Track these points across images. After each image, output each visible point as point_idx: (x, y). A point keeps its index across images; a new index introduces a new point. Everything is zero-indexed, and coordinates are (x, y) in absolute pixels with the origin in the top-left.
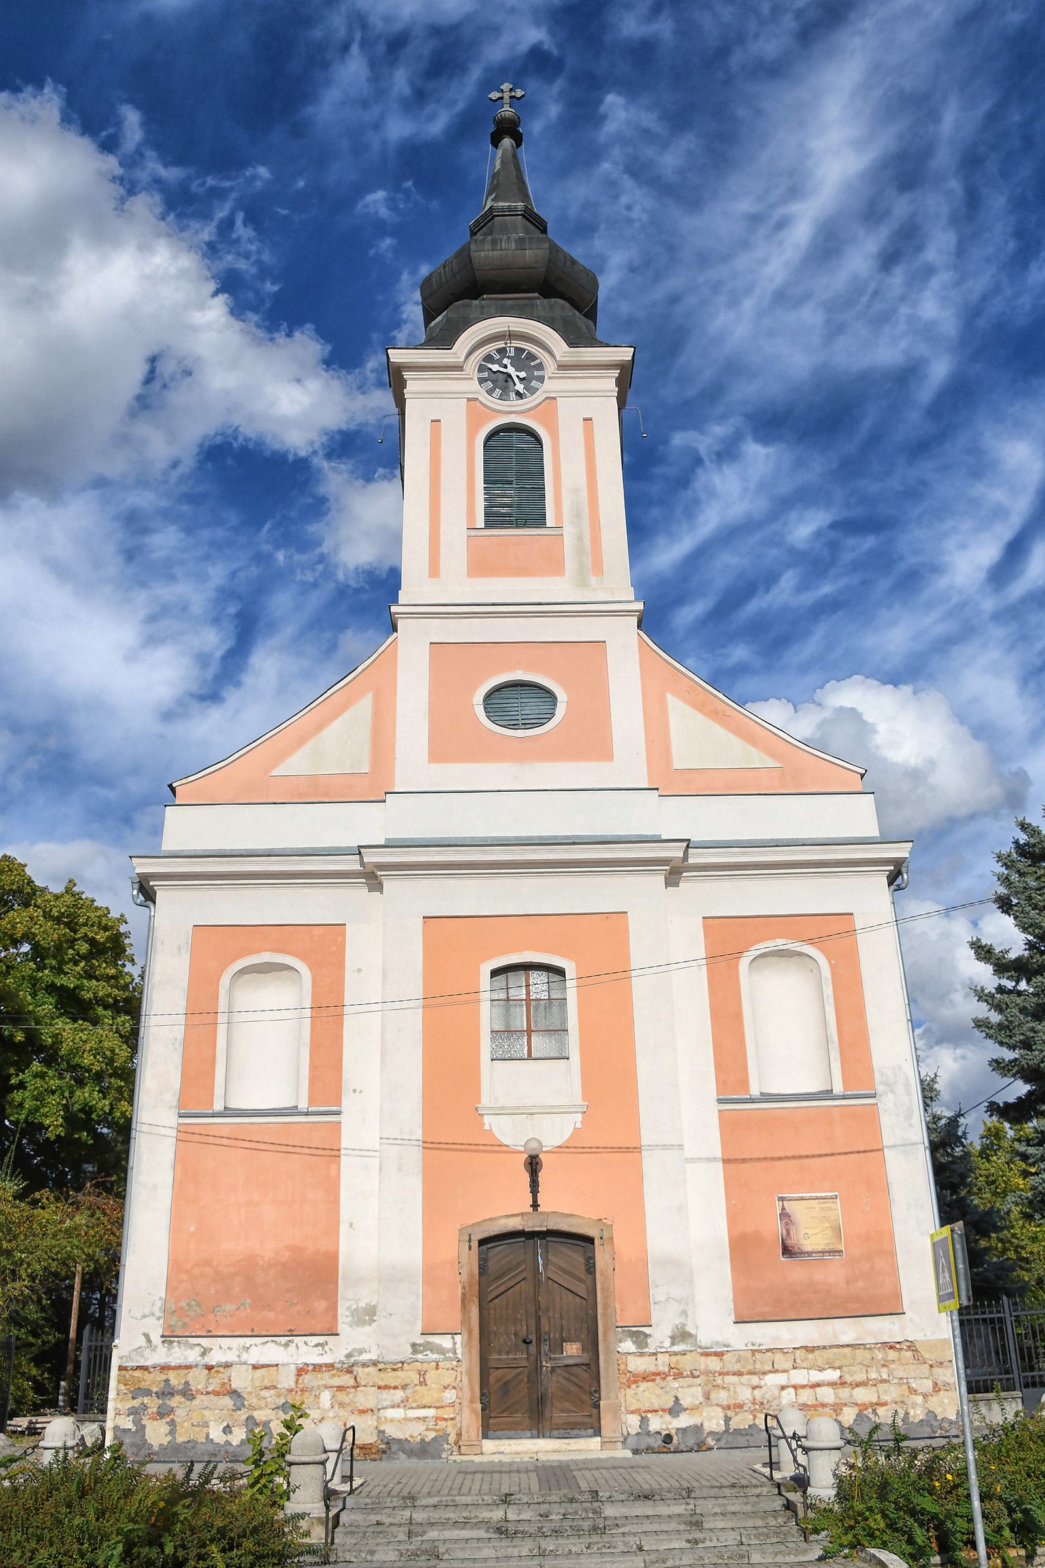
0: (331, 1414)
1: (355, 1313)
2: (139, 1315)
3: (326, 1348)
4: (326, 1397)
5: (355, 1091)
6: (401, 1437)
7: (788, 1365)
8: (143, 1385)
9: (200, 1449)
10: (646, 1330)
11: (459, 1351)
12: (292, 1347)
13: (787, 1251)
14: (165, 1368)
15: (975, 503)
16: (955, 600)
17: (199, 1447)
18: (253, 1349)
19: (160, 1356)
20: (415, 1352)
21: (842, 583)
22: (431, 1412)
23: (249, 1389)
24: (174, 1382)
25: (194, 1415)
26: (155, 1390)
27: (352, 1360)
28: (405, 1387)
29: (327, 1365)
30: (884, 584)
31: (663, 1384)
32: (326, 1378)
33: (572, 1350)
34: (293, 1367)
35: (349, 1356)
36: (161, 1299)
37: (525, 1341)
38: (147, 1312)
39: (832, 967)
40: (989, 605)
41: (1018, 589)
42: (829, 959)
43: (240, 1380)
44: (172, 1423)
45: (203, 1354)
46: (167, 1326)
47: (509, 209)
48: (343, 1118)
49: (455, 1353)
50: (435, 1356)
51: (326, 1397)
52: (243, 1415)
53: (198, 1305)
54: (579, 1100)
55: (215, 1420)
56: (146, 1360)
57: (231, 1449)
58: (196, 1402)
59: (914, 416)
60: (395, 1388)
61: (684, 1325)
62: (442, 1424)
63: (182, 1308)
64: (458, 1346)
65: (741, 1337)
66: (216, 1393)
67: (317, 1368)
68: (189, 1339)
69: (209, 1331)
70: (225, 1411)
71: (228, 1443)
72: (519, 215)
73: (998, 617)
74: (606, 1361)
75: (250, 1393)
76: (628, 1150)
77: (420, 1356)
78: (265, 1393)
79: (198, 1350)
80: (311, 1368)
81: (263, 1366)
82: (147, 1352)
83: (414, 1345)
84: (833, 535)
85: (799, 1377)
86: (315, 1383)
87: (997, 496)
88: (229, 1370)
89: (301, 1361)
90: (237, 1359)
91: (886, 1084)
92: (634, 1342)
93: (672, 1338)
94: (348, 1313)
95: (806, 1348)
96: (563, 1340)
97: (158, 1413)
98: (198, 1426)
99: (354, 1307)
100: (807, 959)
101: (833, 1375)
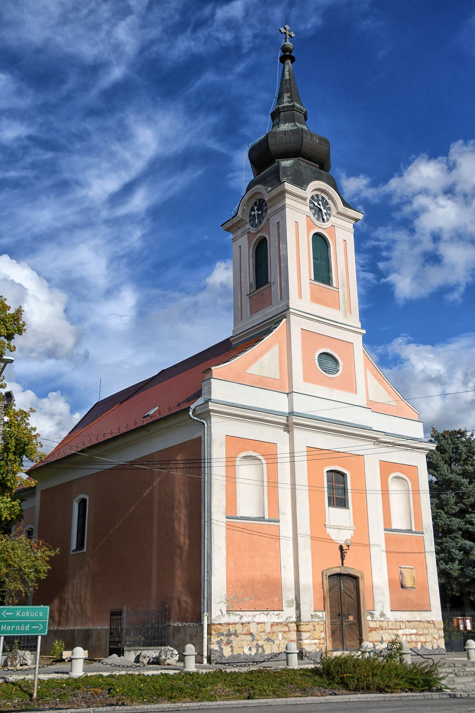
0: (282, 642)
1: (288, 602)
2: (218, 602)
3: (280, 616)
4: (280, 635)
5: (283, 513)
6: (310, 651)
7: (404, 627)
8: (221, 632)
9: (242, 657)
10: (373, 612)
11: (324, 618)
12: (269, 615)
13: (402, 586)
14: (228, 624)
15: (112, 154)
16: (87, 204)
17: (241, 656)
18: (257, 616)
19: (226, 619)
20: (312, 618)
21: (23, 173)
22: (317, 641)
23: (256, 633)
24: (231, 630)
25: (239, 643)
26: (225, 633)
27: (288, 621)
28: (309, 631)
29: (280, 623)
30: (47, 182)
31: (378, 632)
32: (280, 628)
33: (351, 618)
34: (270, 624)
35: (287, 619)
36: (225, 595)
37: (338, 615)
38: (220, 601)
39: (412, 485)
40: (105, 214)
41: (122, 211)
42: (411, 482)
43: (253, 629)
44: (232, 647)
45: (241, 618)
46: (227, 607)
47: (301, 109)
48: (280, 524)
49: (323, 619)
50: (318, 620)
51: (280, 635)
52: (255, 643)
53: (237, 598)
54: (352, 525)
55: (246, 645)
56: (221, 621)
57: (251, 657)
58: (239, 638)
59: (94, 93)
60: (307, 632)
61: (383, 611)
62: (321, 646)
63: (231, 599)
64: (324, 616)
65: (391, 616)
66: (245, 634)
67: (277, 624)
68: (236, 612)
69: (241, 609)
70: (249, 642)
71: (250, 654)
72: (302, 113)
73: (107, 222)
74: (365, 623)
75: (256, 634)
76: (365, 545)
77: (314, 620)
78: (262, 634)
79: (239, 617)
80: (275, 624)
81: (261, 623)
82: (222, 618)
83: (312, 615)
84: (26, 142)
85: (407, 631)
86: (277, 630)
87: (127, 155)
88: (249, 624)
89: (272, 621)
90: (252, 620)
91: (426, 530)
92: (371, 616)
93: (380, 615)
94: (286, 602)
95: (408, 621)
96: (349, 615)
97: (227, 643)
98: (241, 648)
99: (287, 600)
100: (404, 481)
101: (414, 631)
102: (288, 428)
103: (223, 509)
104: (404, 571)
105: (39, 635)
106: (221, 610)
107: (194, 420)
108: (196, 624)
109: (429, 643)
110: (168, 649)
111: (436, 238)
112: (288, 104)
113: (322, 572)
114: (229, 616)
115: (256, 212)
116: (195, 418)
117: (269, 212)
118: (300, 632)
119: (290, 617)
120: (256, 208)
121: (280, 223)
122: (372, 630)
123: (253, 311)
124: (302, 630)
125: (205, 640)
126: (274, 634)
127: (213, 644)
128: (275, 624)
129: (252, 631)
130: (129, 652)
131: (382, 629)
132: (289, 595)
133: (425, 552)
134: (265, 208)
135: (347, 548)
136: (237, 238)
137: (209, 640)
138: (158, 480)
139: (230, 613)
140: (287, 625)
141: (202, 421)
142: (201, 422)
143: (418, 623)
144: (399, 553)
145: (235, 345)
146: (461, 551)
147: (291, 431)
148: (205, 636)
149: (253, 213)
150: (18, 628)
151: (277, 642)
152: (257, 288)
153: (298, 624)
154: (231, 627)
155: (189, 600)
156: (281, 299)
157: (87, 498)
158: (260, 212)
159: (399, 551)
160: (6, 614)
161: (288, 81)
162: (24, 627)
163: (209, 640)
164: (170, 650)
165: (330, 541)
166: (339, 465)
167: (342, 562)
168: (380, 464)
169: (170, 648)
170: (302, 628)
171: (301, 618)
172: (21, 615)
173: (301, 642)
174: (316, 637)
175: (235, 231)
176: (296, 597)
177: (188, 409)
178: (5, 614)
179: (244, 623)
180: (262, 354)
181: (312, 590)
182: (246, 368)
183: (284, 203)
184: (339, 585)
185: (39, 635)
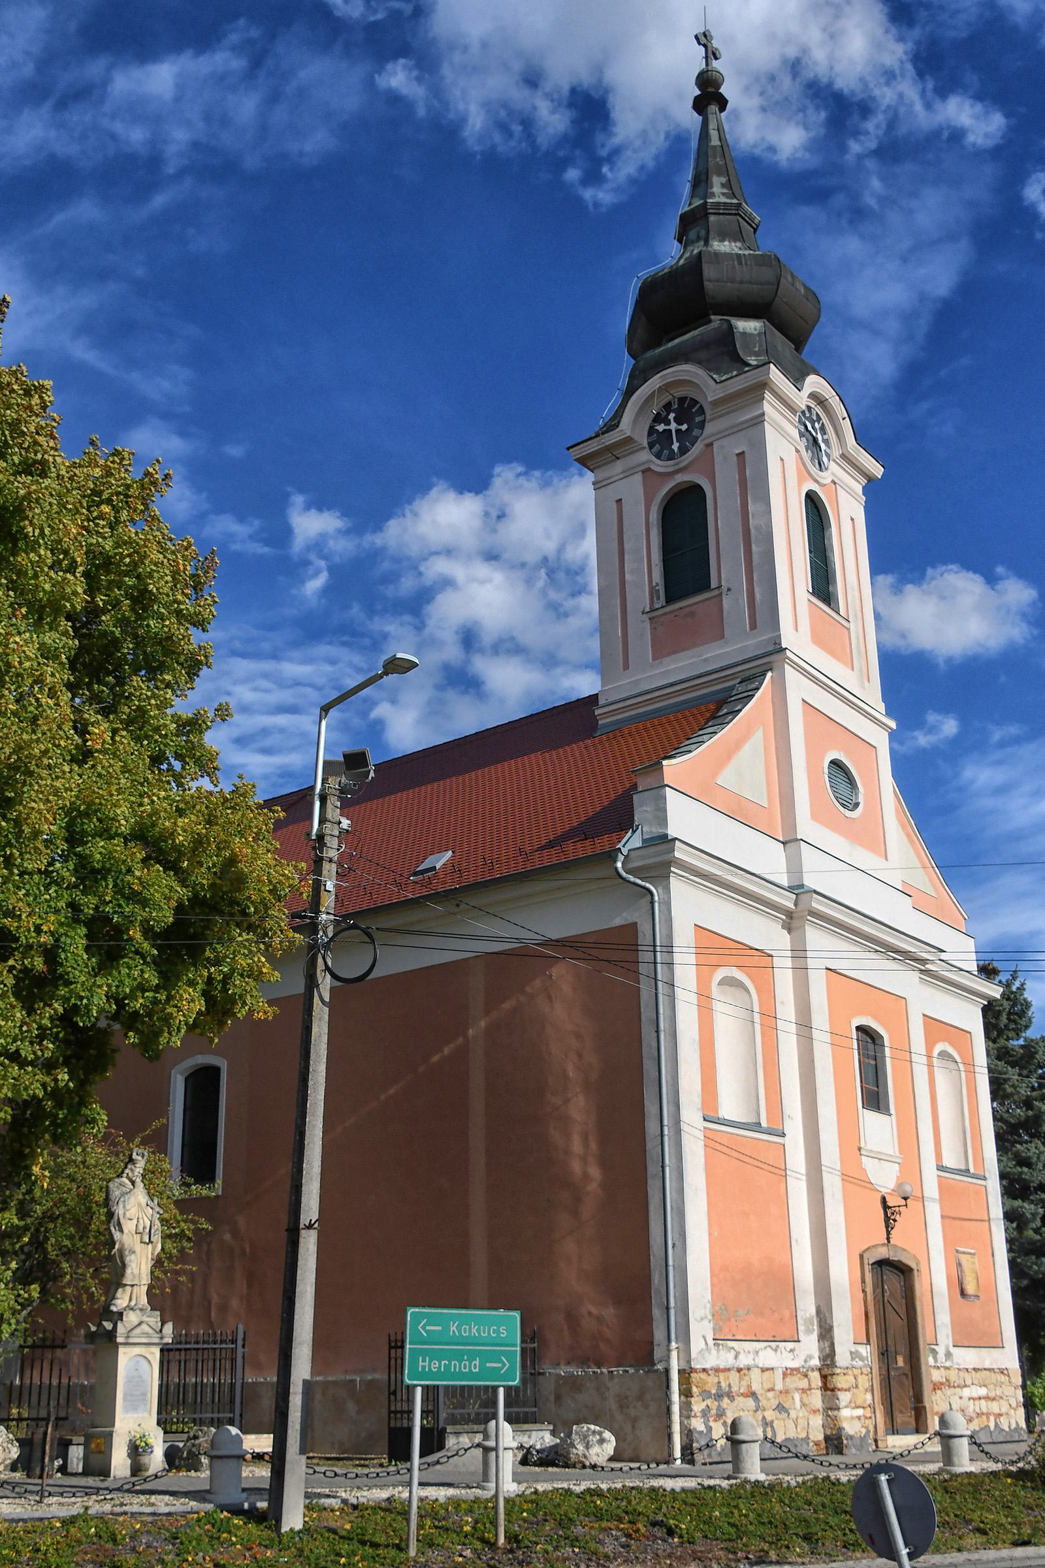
2: (699, 1318)
4: (797, 1396)
14: (717, 1370)
18: (761, 1353)
20: (853, 1359)
43: (756, 1381)
45: (736, 1358)
50: (861, 1363)
51: (797, 1396)
75: (761, 1395)
77: (854, 1363)
78: (770, 1395)
101: (983, 1392)
102: (791, 921)
103: (698, 1100)
104: (964, 1259)
105: (499, 1386)
106: (704, 1337)
107: (629, 882)
108: (637, 1371)
109: (1004, 1416)
110: (588, 1428)
111: (469, 638)
112: (723, 200)
113: (861, 1257)
114: (718, 1351)
115: (673, 426)
116: (632, 878)
117: (710, 428)
118: (833, 1390)
119: (810, 1357)
120: (672, 416)
121: (747, 457)
122: (937, 1387)
123: (662, 649)
124: (839, 1386)
125: (676, 1409)
126: (788, 1395)
127: (695, 1416)
128: (789, 1371)
129: (756, 1387)
130: (457, 1437)
131: (949, 1386)
132: (807, 1307)
133: (989, 1220)
134: (698, 419)
135: (903, 1202)
136: (609, 481)
137: (686, 1408)
138: (483, 1024)
139: (719, 1345)
140: (806, 1376)
141: (648, 885)
142: (644, 887)
143: (988, 1372)
144: (954, 1218)
145: (606, 725)
146: (1012, 1222)
147: (797, 928)
148: (675, 1397)
149: (661, 427)
150: (455, 1364)
151: (793, 1414)
152: (670, 600)
153: (826, 1371)
154: (722, 1375)
155: (609, 1312)
156: (753, 626)
157: (223, 1064)
158: (684, 427)
159: (954, 1216)
160: (428, 1328)
161: (719, 149)
162: (467, 1363)
163: (686, 1408)
164: (594, 1432)
165: (867, 1185)
166: (875, 1017)
167: (888, 1233)
168: (924, 1021)
169: (592, 1427)
170: (840, 1381)
171: (837, 1358)
172: (460, 1332)
173: (835, 1413)
174: (859, 1402)
175: (604, 465)
176: (818, 1312)
177: (612, 855)
178: (424, 1327)
179: (741, 1369)
180: (738, 745)
181: (848, 1295)
182: (715, 774)
183: (760, 412)
184: (880, 1286)
185: (499, 1386)
